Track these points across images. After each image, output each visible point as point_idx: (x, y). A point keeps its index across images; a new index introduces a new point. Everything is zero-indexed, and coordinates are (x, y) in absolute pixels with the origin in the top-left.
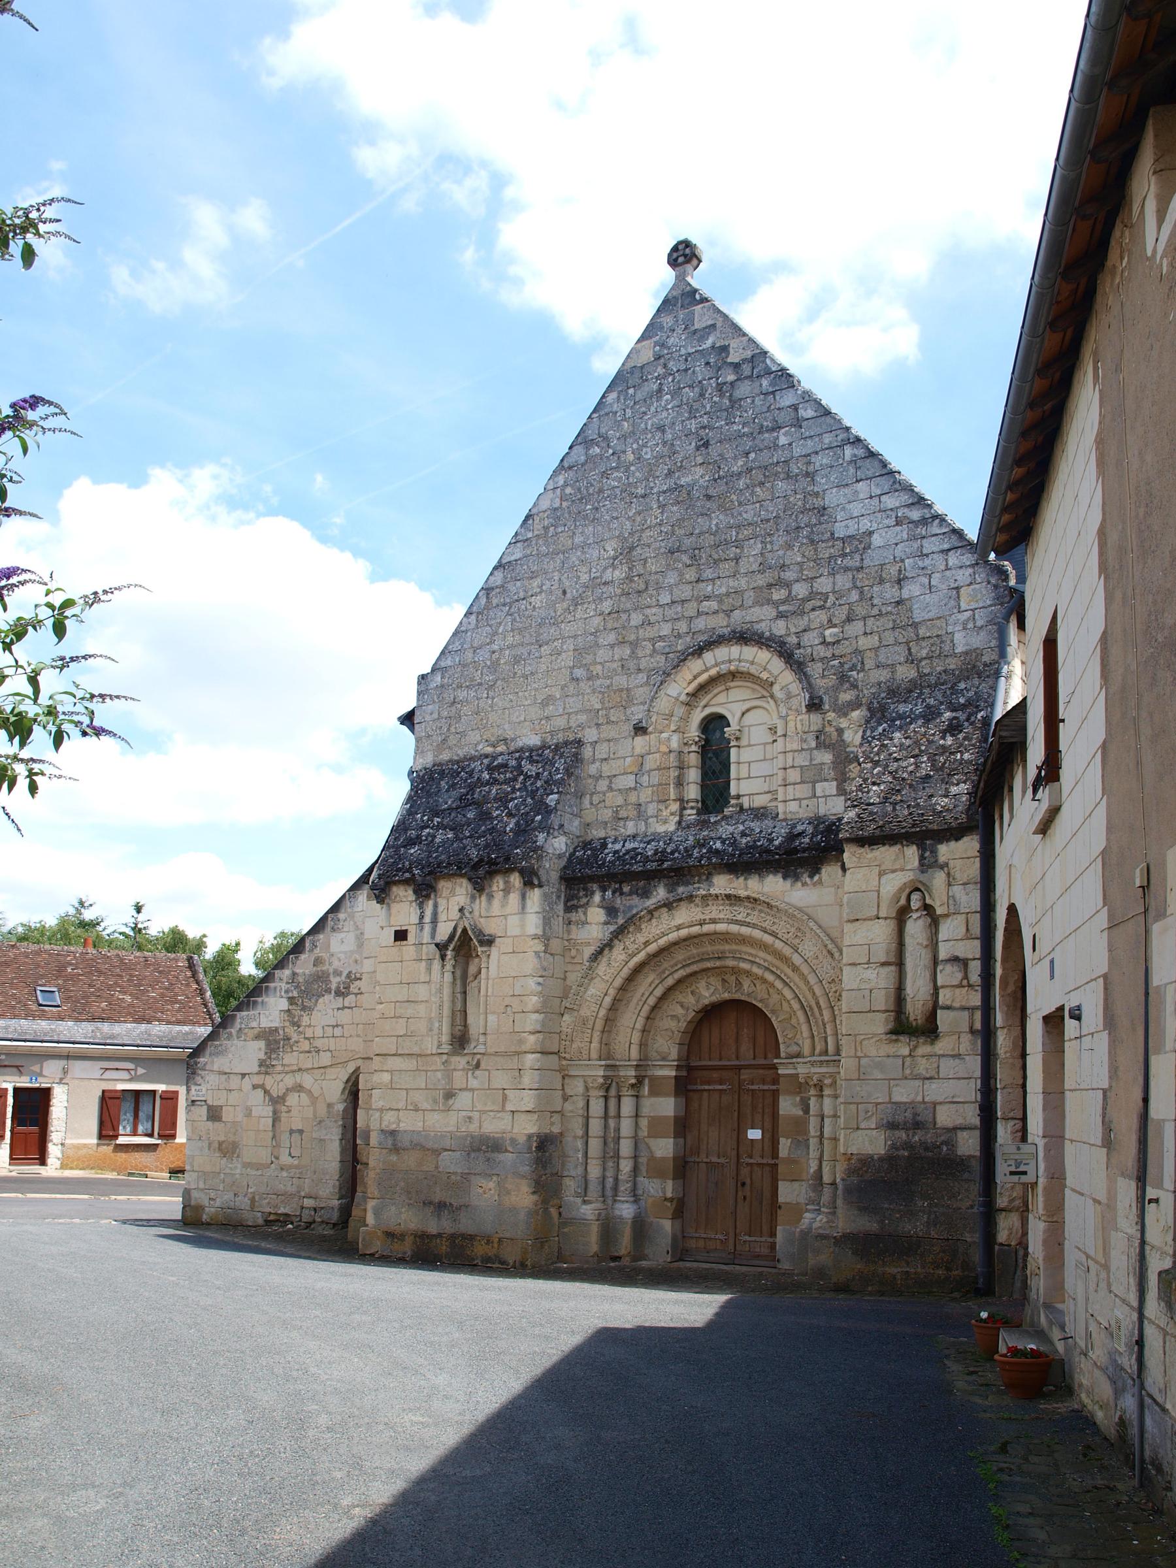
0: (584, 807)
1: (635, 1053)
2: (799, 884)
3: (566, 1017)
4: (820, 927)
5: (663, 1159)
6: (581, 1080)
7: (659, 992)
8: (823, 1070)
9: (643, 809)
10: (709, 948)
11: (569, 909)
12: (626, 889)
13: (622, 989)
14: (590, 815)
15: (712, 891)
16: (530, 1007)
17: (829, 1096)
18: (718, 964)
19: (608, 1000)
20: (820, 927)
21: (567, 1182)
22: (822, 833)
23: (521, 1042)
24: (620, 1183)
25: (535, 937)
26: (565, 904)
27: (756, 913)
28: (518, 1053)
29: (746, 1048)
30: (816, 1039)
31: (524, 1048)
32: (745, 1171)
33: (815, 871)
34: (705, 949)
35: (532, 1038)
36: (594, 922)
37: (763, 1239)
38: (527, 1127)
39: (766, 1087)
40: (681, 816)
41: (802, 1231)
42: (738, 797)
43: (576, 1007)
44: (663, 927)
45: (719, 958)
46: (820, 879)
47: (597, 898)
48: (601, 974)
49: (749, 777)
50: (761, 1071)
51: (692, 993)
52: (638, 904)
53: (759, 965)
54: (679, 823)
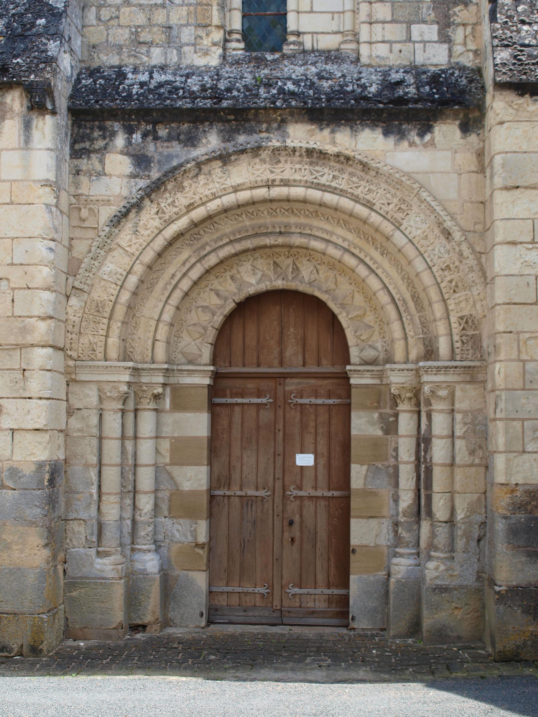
0: (87, 21)
1: (160, 353)
2: (406, 144)
3: (73, 301)
4: (435, 199)
5: (194, 493)
6: (94, 387)
7: (195, 274)
8: (440, 378)
9: (174, 33)
10: (268, 220)
12: (162, 132)
14: (96, 34)
15: (290, 143)
16: (38, 282)
17: (441, 411)
18: (281, 240)
19: (133, 280)
20: (435, 199)
21: (75, 526)
22: (428, 83)
23: (25, 330)
24: (140, 526)
25: (46, 183)
26: (72, 147)
27: (346, 176)
28: (21, 347)
29: (292, 350)
30: (411, 341)
31: (30, 339)
32: (293, 506)
33: (426, 129)
34: (261, 221)
35: (42, 326)
36: (115, 172)
37: (318, 591)
38: (36, 451)
39: (319, 401)
40: (225, 49)
41: (398, 581)
42: (298, 34)
43: (86, 288)
44: (215, 187)
45: (281, 233)
46: (433, 139)
47: (120, 141)
48: (124, 244)
49: (311, 12)
50: (313, 381)
51: (232, 278)
52: (178, 153)
53: (336, 245)
54: (224, 57)
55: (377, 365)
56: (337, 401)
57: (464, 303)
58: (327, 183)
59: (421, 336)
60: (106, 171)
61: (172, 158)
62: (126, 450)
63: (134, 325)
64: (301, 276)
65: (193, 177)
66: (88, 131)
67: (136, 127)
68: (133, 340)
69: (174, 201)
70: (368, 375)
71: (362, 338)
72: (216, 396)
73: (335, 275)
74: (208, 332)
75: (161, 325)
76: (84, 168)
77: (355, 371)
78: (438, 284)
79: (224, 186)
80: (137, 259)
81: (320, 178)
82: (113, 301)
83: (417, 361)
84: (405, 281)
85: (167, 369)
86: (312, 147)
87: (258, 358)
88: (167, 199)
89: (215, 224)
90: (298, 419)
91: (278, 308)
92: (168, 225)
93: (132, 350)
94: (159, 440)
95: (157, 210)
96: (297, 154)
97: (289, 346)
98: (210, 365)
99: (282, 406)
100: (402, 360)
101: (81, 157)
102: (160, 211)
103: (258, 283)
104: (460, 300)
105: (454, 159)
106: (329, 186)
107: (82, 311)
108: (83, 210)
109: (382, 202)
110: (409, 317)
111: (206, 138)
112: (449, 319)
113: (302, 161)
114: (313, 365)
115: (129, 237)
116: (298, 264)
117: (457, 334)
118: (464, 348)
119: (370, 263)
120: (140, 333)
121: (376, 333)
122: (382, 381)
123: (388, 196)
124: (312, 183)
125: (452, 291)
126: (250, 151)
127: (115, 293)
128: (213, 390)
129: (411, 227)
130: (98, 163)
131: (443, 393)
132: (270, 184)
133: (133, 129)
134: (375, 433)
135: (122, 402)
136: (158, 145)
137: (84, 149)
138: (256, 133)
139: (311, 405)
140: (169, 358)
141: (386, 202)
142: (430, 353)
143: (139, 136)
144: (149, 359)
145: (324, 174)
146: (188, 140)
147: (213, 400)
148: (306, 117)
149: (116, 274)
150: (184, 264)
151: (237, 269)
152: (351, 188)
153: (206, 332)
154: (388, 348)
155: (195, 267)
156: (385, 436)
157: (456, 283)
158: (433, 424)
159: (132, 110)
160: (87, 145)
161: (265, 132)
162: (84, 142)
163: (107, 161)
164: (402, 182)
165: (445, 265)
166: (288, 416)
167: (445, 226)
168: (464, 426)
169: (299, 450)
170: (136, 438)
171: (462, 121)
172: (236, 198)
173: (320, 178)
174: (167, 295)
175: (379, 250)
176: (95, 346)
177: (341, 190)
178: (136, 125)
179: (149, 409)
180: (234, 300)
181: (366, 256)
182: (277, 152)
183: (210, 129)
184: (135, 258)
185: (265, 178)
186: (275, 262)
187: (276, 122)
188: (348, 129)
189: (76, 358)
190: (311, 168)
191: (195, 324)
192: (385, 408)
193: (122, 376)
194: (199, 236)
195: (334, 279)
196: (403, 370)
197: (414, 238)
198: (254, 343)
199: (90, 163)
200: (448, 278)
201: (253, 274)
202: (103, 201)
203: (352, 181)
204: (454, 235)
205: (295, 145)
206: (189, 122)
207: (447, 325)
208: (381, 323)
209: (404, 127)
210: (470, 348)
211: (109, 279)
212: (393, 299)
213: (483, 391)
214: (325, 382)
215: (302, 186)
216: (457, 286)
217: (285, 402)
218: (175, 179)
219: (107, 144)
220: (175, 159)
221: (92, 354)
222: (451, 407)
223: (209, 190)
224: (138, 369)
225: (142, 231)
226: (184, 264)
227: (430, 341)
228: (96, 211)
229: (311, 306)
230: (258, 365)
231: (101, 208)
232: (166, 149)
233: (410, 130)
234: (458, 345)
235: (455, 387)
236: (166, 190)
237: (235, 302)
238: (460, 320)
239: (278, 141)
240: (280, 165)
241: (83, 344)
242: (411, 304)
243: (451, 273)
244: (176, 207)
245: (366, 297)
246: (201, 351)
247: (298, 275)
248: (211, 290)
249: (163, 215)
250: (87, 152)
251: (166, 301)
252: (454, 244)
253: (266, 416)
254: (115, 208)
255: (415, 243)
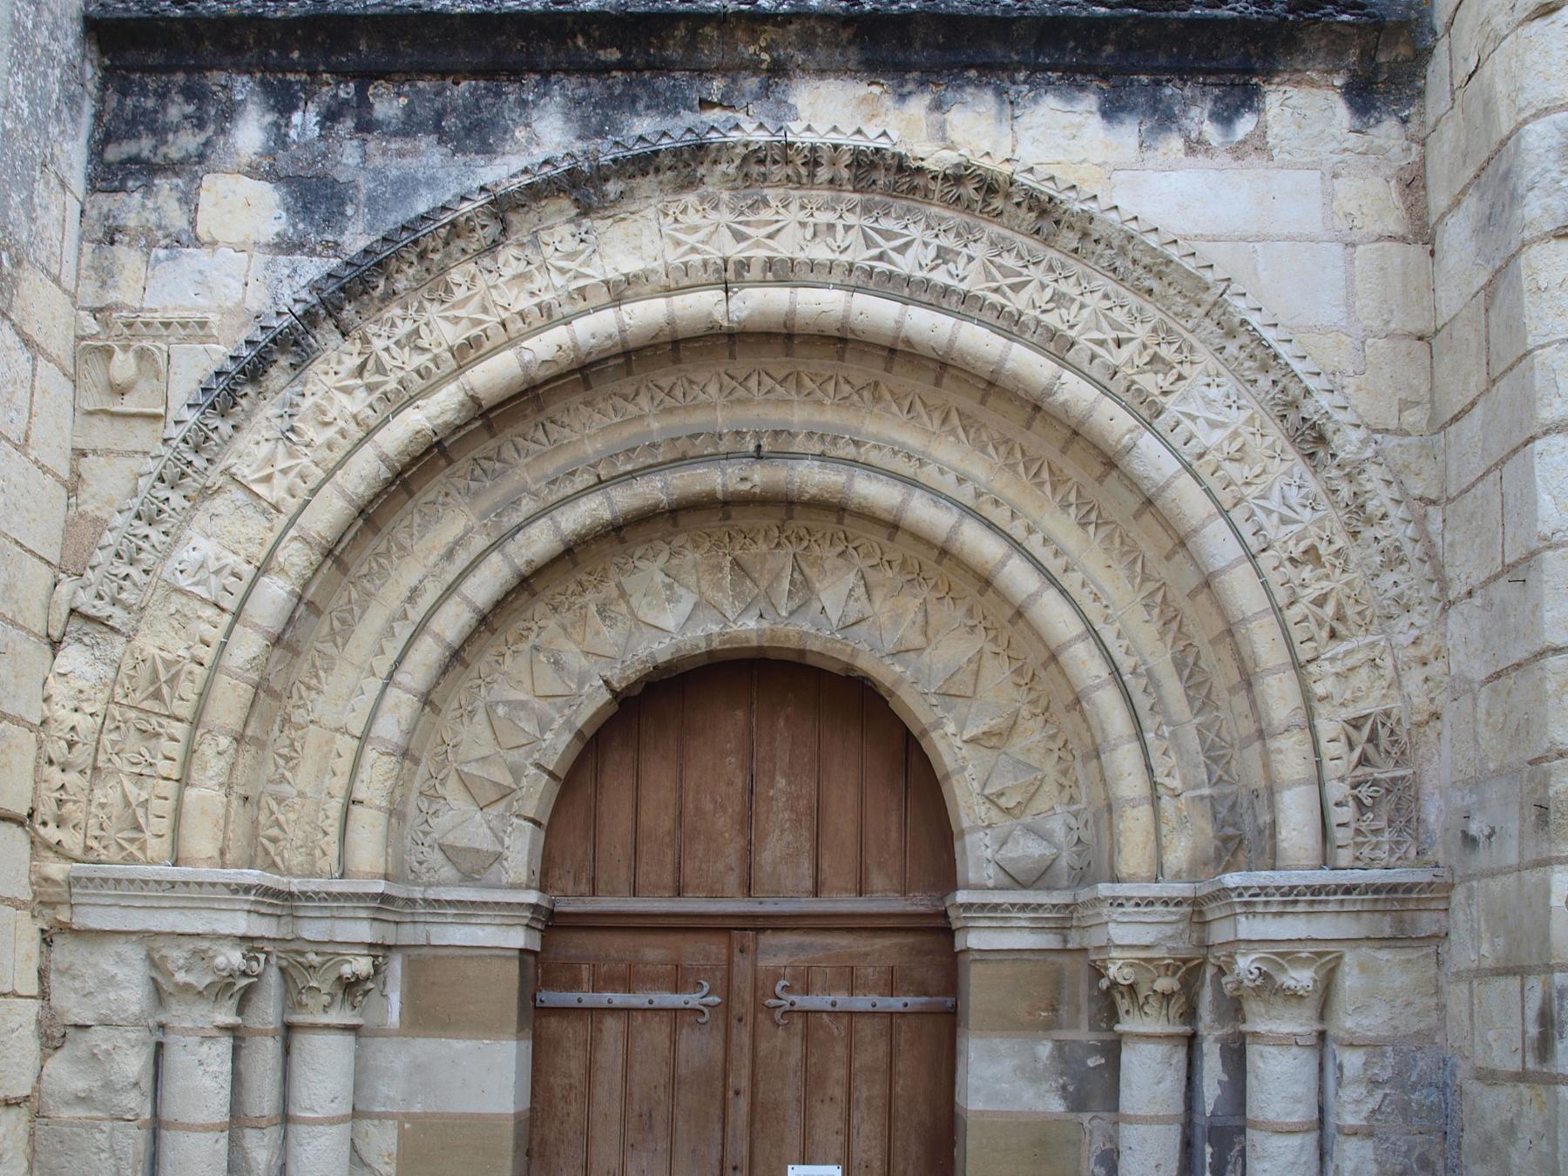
1: (369, 849)
2: (1176, 143)
3: (73, 657)
7: (485, 585)
10: (722, 419)
11: (108, 175)
13: (335, 554)
15: (798, 134)
18: (760, 477)
19: (275, 593)
27: (980, 250)
29: (780, 845)
33: (1239, 97)
34: (697, 419)
39: (862, 1002)
43: (119, 617)
44: (551, 286)
46: (1261, 132)
47: (250, 133)
48: (246, 472)
50: (842, 942)
53: (935, 493)
55: (1049, 889)
56: (914, 1001)
57: (1364, 671)
58: (919, 275)
59: (1206, 791)
60: (201, 230)
61: (415, 190)
62: (245, 1159)
63: (285, 751)
64: (816, 606)
65: (479, 253)
66: (150, 103)
67: (303, 89)
68: (280, 800)
69: (417, 332)
70: (1023, 919)
71: (1003, 802)
72: (549, 983)
73: (925, 602)
74: (524, 781)
75: (370, 754)
76: (131, 221)
77: (983, 906)
78: (1278, 611)
79: (581, 283)
80: (291, 523)
81: (894, 255)
82: (207, 662)
83: (1194, 871)
84: (1156, 611)
85: (384, 898)
86: (872, 145)
87: (678, 868)
88: (393, 325)
89: (549, 426)
90: (795, 1058)
91: (740, 714)
92: (395, 413)
93: (275, 832)
94: (365, 1124)
95: (358, 361)
96: (823, 173)
97: (761, 833)
98: (528, 887)
99: (749, 1019)
100: (1144, 871)
101: (122, 189)
102: (371, 362)
103: (682, 629)
104: (1350, 662)
105: (1330, 196)
106: (926, 284)
107: (103, 696)
108: (119, 356)
109: (1097, 335)
110: (1166, 730)
111: (528, 125)
112: (1312, 728)
113: (839, 201)
114: (846, 890)
115: (266, 448)
116: (807, 570)
117: (1342, 779)
118: (1363, 827)
119: (1043, 554)
120: (303, 778)
121: (1049, 788)
122: (1065, 941)
123: (1119, 315)
124: (870, 273)
125: (1325, 634)
126: (668, 161)
127: (216, 636)
128: (538, 969)
129: (1193, 418)
130: (176, 205)
131: (1301, 978)
132: (729, 277)
133: (294, 96)
134: (1040, 1107)
135: (234, 1002)
136: (371, 146)
137: (135, 160)
138: (691, 109)
139: (834, 1014)
140: (401, 862)
141: (1110, 335)
142: (1232, 845)
143: (313, 118)
144: (329, 862)
145: (907, 245)
146: (468, 131)
147: (539, 996)
148: (854, 55)
149: (217, 572)
150: (450, 555)
151: (619, 585)
152: (996, 290)
153: (517, 781)
154: (1087, 836)
155: (482, 566)
156: (1073, 1116)
157: (1340, 606)
158: (1251, 1081)
159: (288, 25)
160: (143, 146)
161: (720, 105)
162: (136, 136)
163: (205, 199)
164: (1169, 262)
165: (1303, 546)
166: (764, 1047)
167: (1308, 409)
168: (1370, 1093)
169: (796, 1154)
170: (285, 1118)
171: (1353, 74)
172: (621, 320)
173: (894, 255)
174: (392, 654)
175: (1072, 510)
176: (140, 812)
177: (965, 298)
178: (303, 84)
179: (327, 1027)
180: (607, 682)
181: (1030, 530)
182: (756, 170)
183: (541, 96)
184: (283, 520)
185: (714, 255)
186: (736, 563)
187: (755, 74)
188: (989, 97)
189: (78, 852)
190: (869, 222)
191: (484, 759)
192: (1074, 1025)
193: (226, 916)
194: (498, 465)
195: (920, 618)
196: (1151, 903)
197: (1201, 456)
198: (667, 823)
199: (150, 204)
200: (1314, 591)
201: (669, 601)
202: (184, 326)
203: (999, 267)
204: (1337, 441)
205: (817, 140)
206: (475, 73)
207: (1308, 747)
208: (1063, 754)
209: (1168, 91)
210: (1383, 824)
211: (196, 590)
212: (1116, 672)
213: (1432, 971)
214: (880, 943)
215: (836, 287)
216: (1340, 617)
217: (758, 1006)
218: (422, 256)
219: (206, 144)
220: (423, 191)
221: (132, 841)
222: (1318, 1027)
223: (532, 294)
224: (291, 894)
225: (310, 432)
226: (450, 555)
227: (1233, 807)
228: (161, 359)
229: (839, 702)
230: (679, 892)
231: (176, 349)
232: (396, 161)
233: (1188, 103)
234: (1347, 813)
235: (1340, 957)
236: (390, 295)
237: (612, 691)
238: (1350, 730)
239: (761, 126)
240: (766, 214)
241: (103, 806)
242: (1173, 688)
243: (1320, 571)
244: (424, 350)
245: (1018, 672)
246: (502, 843)
247: (805, 604)
248: (536, 648)
249: (378, 378)
250: (147, 170)
251: (390, 676)
252: (1334, 473)
253: (698, 1047)
254: (222, 348)
255: (1204, 473)
